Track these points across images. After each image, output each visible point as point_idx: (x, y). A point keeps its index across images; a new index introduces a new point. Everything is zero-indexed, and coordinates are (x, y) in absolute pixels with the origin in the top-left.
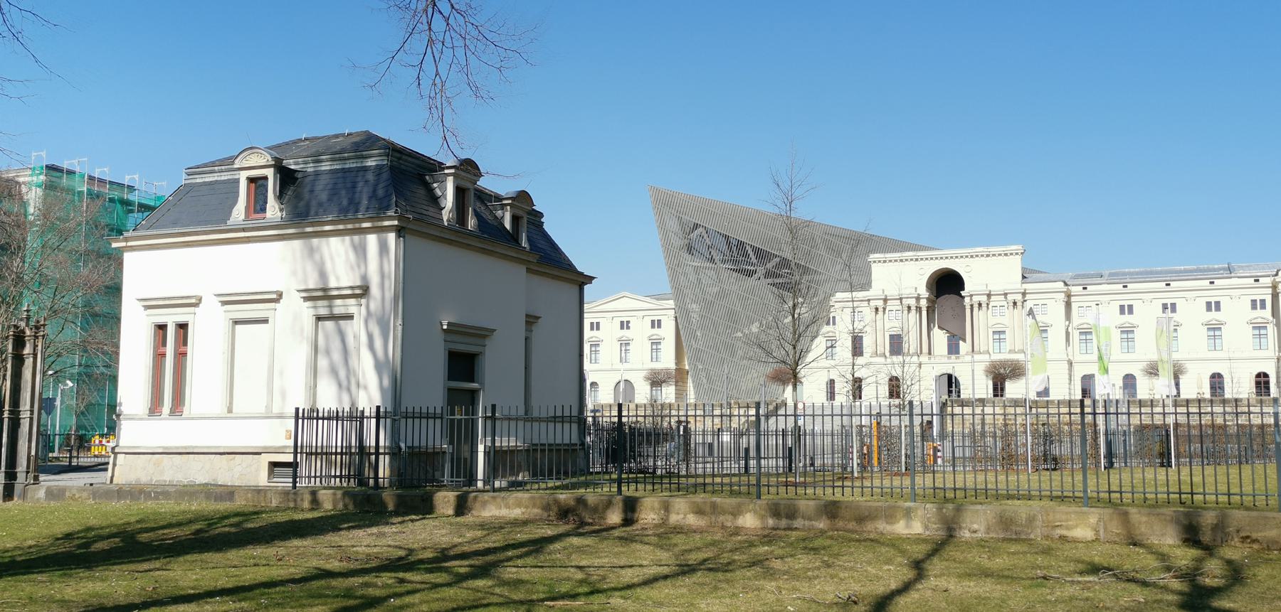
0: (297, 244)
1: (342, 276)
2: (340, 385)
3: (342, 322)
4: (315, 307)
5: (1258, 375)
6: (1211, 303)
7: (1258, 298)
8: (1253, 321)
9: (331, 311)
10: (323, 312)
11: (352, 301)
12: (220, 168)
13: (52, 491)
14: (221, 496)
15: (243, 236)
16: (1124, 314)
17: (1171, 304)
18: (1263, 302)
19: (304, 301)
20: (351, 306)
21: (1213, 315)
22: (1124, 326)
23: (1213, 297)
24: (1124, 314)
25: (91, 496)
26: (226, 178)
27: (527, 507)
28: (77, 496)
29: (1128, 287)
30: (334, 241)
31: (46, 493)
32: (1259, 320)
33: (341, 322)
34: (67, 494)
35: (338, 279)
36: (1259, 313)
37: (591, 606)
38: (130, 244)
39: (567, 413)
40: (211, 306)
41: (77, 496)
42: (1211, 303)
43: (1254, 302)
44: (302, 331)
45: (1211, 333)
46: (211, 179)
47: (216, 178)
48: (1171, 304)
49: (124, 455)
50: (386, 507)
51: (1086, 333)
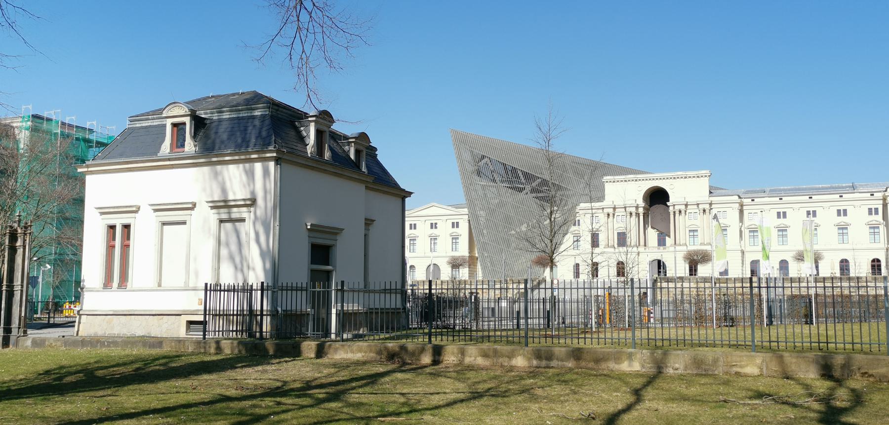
0: (206, 169)
1: (238, 191)
2: (236, 268)
3: (237, 224)
4: (219, 213)
5: (873, 261)
6: (840, 210)
7: (873, 207)
8: (869, 223)
9: (230, 216)
10: (224, 216)
11: (245, 209)
12: (153, 116)
13: (36, 341)
14: (154, 345)
15: (168, 164)
16: (780, 218)
17: (813, 211)
18: (876, 210)
19: (211, 209)
20: (244, 213)
21: (842, 219)
22: (780, 226)
23: (842, 206)
24: (780, 218)
25: (63, 344)
26: (157, 124)
27: (365, 352)
28: (53, 345)
29: (783, 199)
30: (232, 167)
31: (32, 342)
32: (874, 222)
33: (236, 223)
34: (47, 343)
35: (234, 194)
36: (874, 217)
37: (410, 421)
38: (90, 169)
39: (393, 287)
40: (146, 212)
41: (53, 345)
42: (840, 210)
43: (870, 210)
44: (210, 230)
45: (841, 231)
46: (146, 125)
47: (150, 124)
48: (813, 211)
49: (86, 316)
50: (268, 352)
51: (754, 231)
